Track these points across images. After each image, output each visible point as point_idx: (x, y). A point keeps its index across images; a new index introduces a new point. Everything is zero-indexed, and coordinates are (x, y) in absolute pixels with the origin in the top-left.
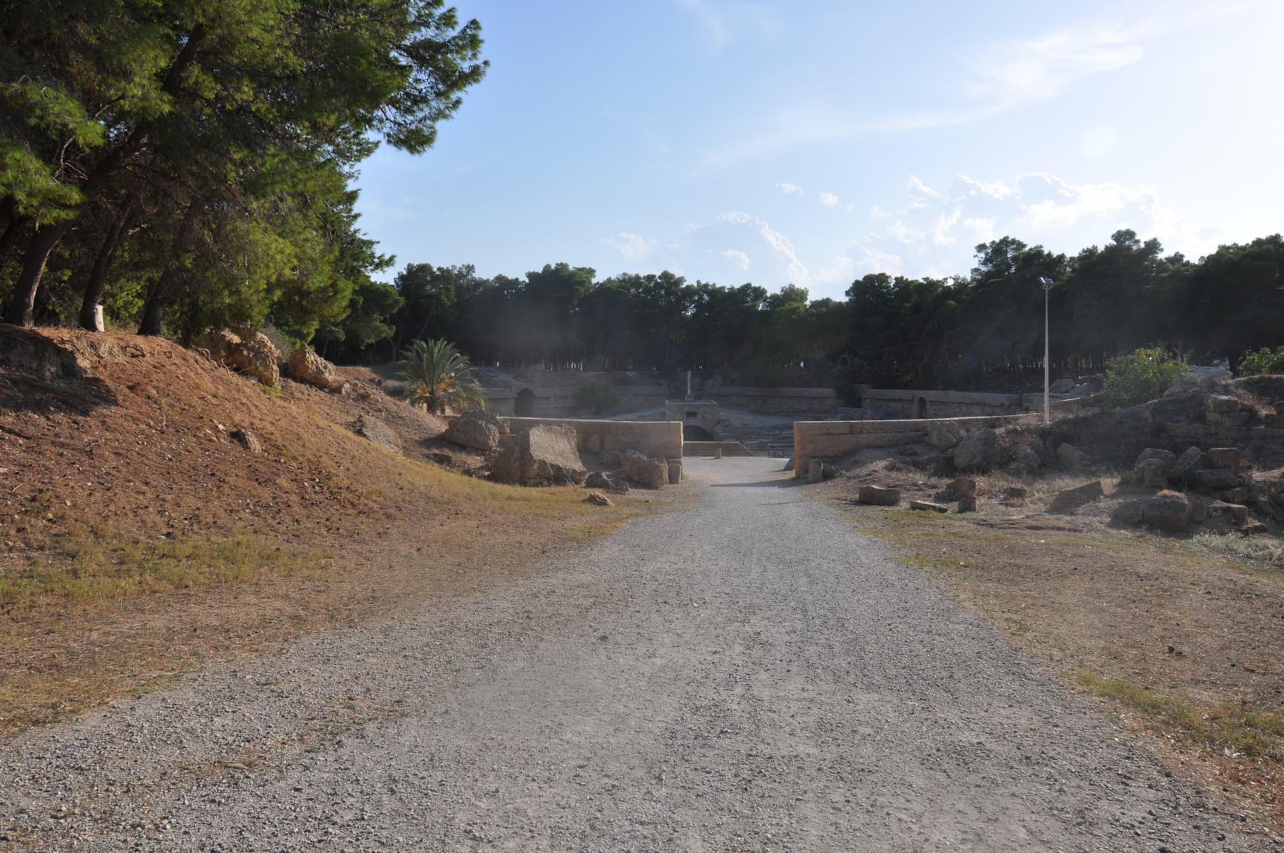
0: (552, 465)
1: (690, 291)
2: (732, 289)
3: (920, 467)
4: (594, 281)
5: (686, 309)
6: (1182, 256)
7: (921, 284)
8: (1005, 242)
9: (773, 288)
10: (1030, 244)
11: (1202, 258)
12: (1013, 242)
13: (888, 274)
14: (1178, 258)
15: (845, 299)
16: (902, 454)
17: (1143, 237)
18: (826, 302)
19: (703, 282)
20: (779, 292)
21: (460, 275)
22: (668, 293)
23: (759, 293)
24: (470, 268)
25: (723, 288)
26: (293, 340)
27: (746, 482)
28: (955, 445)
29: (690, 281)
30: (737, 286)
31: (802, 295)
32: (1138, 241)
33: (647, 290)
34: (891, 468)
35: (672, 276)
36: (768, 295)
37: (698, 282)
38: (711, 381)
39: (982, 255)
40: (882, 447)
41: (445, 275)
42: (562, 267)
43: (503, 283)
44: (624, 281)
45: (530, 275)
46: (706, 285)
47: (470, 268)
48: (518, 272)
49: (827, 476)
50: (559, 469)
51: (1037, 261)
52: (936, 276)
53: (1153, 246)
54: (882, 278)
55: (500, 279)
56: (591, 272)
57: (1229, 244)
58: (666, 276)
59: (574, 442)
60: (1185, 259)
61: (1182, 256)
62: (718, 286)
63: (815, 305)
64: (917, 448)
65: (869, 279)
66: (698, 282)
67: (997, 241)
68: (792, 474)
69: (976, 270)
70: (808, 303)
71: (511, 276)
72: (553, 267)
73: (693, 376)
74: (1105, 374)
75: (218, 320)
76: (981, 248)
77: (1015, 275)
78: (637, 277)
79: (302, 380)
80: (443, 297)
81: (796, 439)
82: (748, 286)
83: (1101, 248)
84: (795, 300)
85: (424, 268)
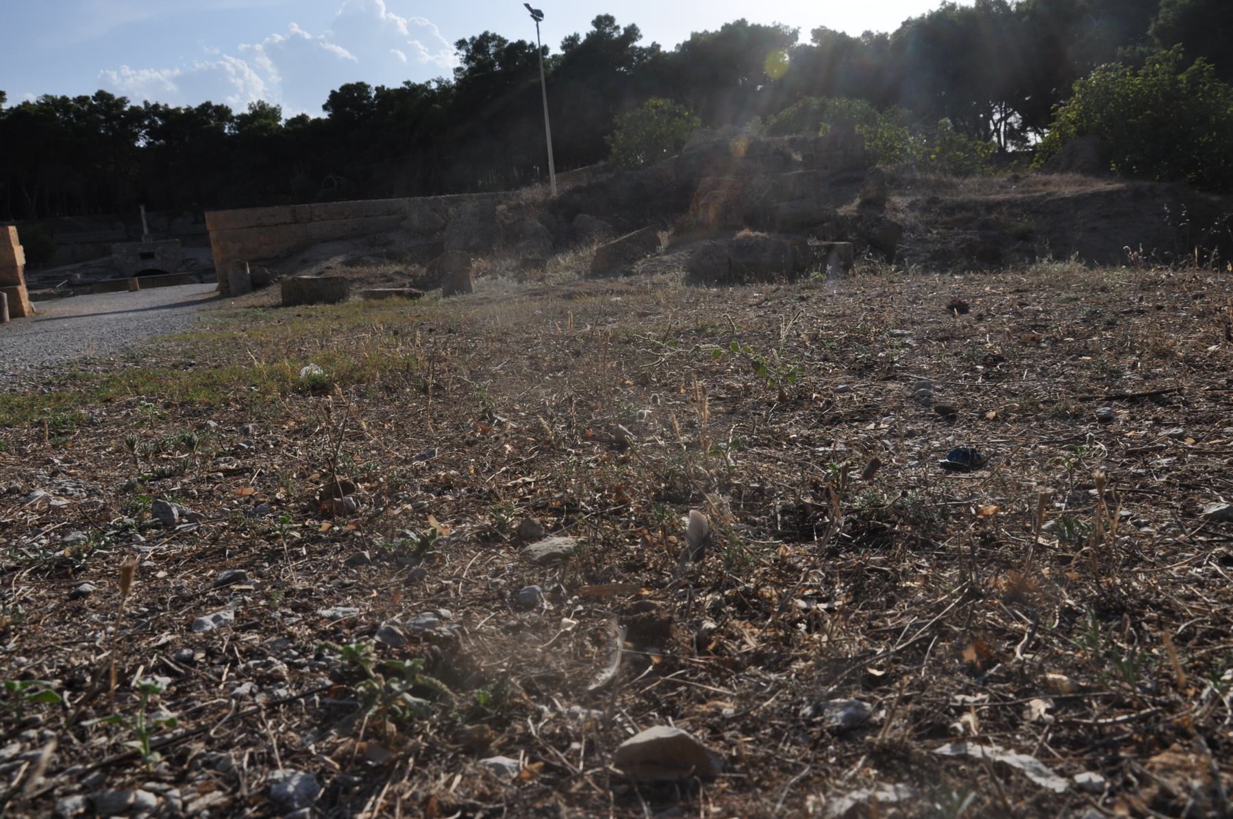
7: (402, 90)
15: (324, 115)
17: (622, 22)
19: (152, 103)
22: (109, 119)
23: (223, 113)
25: (178, 109)
27: (131, 308)
33: (80, 115)
35: (110, 97)
37: (146, 103)
39: (464, 52)
44: (47, 104)
46: (156, 106)
58: (101, 95)
62: (172, 106)
66: (146, 103)
73: (146, 211)
76: (461, 44)
78: (64, 99)
81: (213, 235)
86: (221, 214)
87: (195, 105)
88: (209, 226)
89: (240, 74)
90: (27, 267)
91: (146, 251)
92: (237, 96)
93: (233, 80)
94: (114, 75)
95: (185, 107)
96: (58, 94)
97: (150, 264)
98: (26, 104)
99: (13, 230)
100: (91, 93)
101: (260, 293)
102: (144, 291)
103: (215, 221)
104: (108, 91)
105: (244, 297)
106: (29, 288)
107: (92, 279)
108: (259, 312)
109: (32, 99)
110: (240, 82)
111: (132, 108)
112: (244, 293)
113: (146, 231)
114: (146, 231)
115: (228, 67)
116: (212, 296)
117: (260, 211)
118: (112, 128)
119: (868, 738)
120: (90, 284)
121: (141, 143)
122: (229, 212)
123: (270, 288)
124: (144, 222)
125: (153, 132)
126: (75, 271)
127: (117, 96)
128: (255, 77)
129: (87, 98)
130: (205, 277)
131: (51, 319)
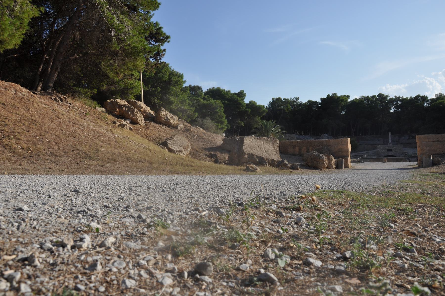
0: (257, 157)
1: (392, 101)
4: (349, 100)
5: (390, 108)
9: (431, 96)
19: (397, 96)
21: (294, 101)
22: (382, 102)
23: (424, 98)
25: (407, 98)
26: (217, 124)
27: (384, 168)
33: (372, 102)
35: (383, 95)
36: (429, 99)
37: (395, 96)
38: (403, 138)
41: (286, 101)
44: (362, 99)
45: (322, 99)
46: (399, 97)
47: (298, 99)
48: (317, 98)
49: (434, 164)
55: (309, 101)
59: (277, 146)
62: (404, 97)
66: (395, 96)
68: (417, 166)
71: (314, 100)
72: (331, 95)
73: (391, 134)
75: (113, 94)
78: (368, 97)
79: (160, 123)
80: (286, 109)
81: (418, 144)
85: (279, 99)
86: (419, 136)
87: (413, 96)
88: (417, 141)
89: (431, 84)
90: (351, 152)
91: (389, 148)
92: (429, 92)
93: (428, 86)
94: (384, 88)
95: (410, 97)
97: (390, 153)
98: (356, 99)
99: (349, 140)
100: (376, 94)
101: (435, 167)
102: (388, 162)
103: (420, 139)
104: (383, 93)
105: (429, 168)
106: (351, 158)
107: (370, 157)
108: (438, 175)
109: (358, 98)
110: (431, 87)
111: (390, 99)
112: (429, 167)
113: (390, 141)
114: (390, 141)
115: (427, 82)
116: (415, 167)
117: (439, 135)
118: (382, 106)
119: (195, 289)
120: (369, 159)
121: (392, 111)
122: (426, 135)
123: (440, 166)
124: (390, 138)
125: (397, 107)
126: (365, 154)
127: (385, 95)
128: (437, 84)
129: (375, 96)
130: (411, 159)
131: (394, 169)
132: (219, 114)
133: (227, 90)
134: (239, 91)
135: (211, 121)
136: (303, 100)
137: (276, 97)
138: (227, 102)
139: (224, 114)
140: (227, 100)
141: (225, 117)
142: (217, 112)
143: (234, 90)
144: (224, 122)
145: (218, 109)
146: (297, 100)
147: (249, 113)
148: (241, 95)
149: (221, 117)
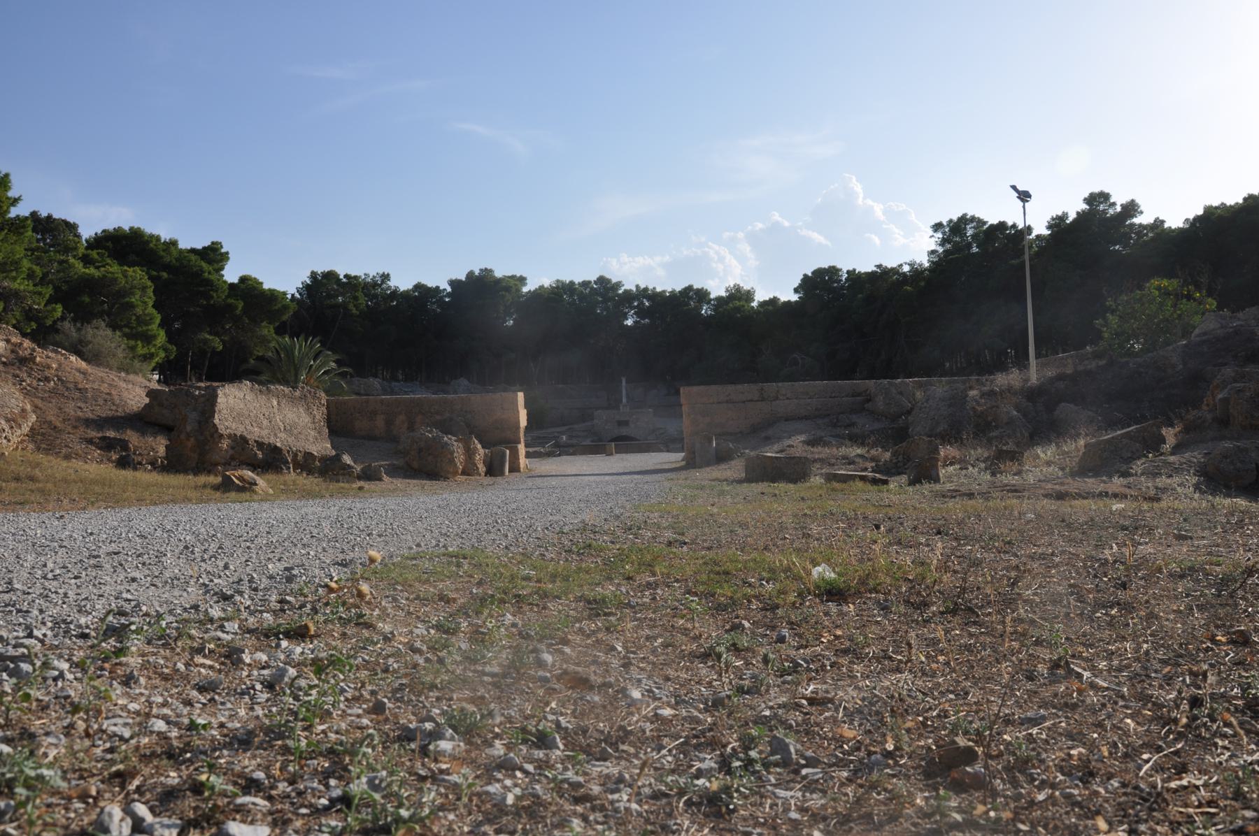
0: (260, 445)
2: (673, 292)
3: (856, 439)
4: (525, 290)
6: (1163, 222)
7: (873, 273)
8: (963, 220)
9: (717, 290)
10: (992, 220)
11: (1187, 220)
12: (973, 219)
13: (839, 266)
14: (1158, 223)
15: (794, 298)
16: (835, 426)
17: (1119, 198)
18: (774, 301)
19: (643, 286)
20: (724, 294)
21: (374, 285)
22: (606, 299)
23: (702, 295)
24: (386, 277)
26: (132, 343)
28: (909, 412)
29: (629, 285)
30: (678, 288)
31: (749, 296)
32: (1114, 204)
33: (582, 297)
34: (811, 443)
35: (609, 281)
36: (712, 296)
37: (637, 286)
39: (940, 235)
40: (806, 418)
41: (352, 283)
42: (487, 272)
43: (423, 293)
44: (557, 287)
45: (453, 283)
46: (646, 289)
47: (386, 277)
48: (439, 279)
50: (276, 450)
51: (1001, 241)
52: (890, 263)
53: (1131, 209)
54: (833, 271)
55: (419, 287)
56: (522, 280)
57: (1216, 203)
59: (320, 414)
60: (1166, 225)
61: (1163, 222)
62: (659, 290)
63: (763, 304)
64: (854, 418)
65: (819, 273)
66: (637, 286)
67: (955, 219)
69: (933, 252)
70: (755, 304)
74: (1105, 318)
76: (937, 227)
77: (978, 257)
78: (572, 283)
80: (351, 306)
82: (690, 288)
83: (1072, 216)
84: (740, 299)
85: (330, 276)
96: (567, 279)
111: (626, 291)
114: (624, 400)
132: (139, 311)
133: (165, 236)
134: (207, 244)
135: (109, 332)
136: (402, 282)
137: (321, 269)
138: (165, 275)
139: (154, 311)
140: (167, 267)
141: (158, 321)
142: (132, 306)
143: (191, 239)
144: (155, 337)
145: (133, 294)
146: (383, 282)
147: (238, 312)
148: (214, 255)
149: (141, 321)
